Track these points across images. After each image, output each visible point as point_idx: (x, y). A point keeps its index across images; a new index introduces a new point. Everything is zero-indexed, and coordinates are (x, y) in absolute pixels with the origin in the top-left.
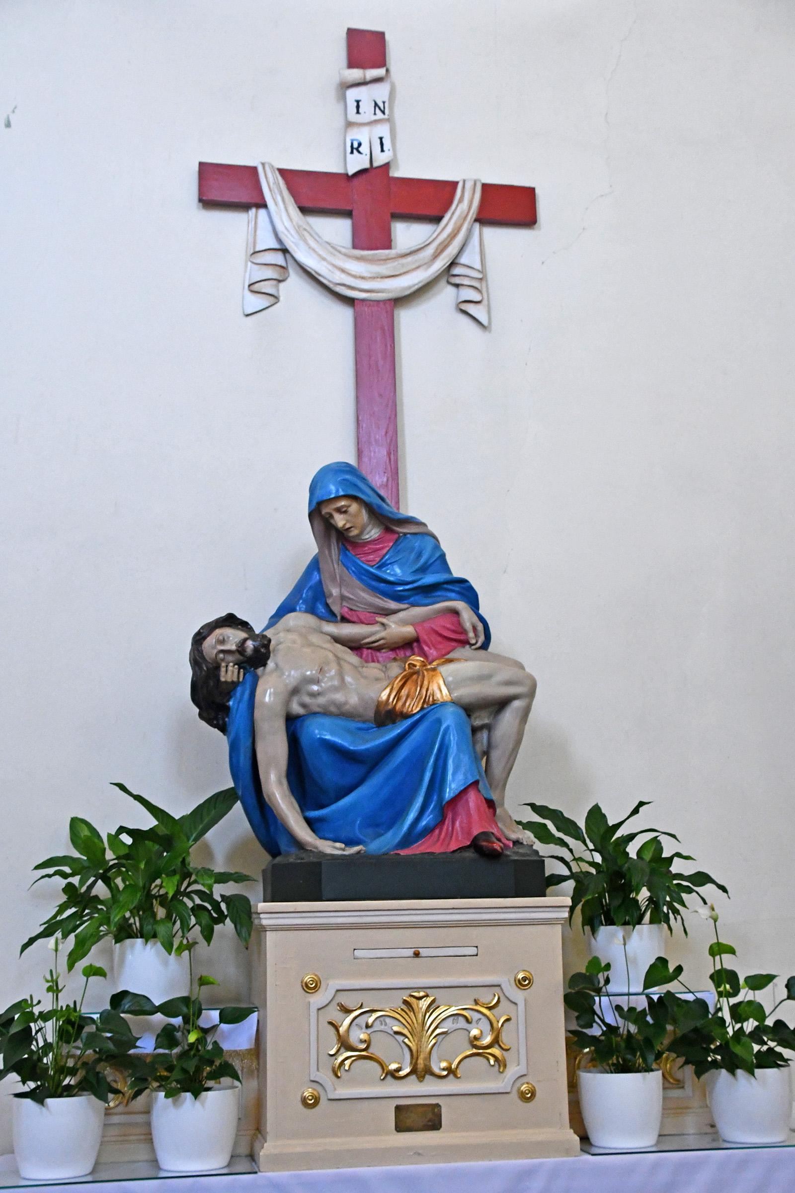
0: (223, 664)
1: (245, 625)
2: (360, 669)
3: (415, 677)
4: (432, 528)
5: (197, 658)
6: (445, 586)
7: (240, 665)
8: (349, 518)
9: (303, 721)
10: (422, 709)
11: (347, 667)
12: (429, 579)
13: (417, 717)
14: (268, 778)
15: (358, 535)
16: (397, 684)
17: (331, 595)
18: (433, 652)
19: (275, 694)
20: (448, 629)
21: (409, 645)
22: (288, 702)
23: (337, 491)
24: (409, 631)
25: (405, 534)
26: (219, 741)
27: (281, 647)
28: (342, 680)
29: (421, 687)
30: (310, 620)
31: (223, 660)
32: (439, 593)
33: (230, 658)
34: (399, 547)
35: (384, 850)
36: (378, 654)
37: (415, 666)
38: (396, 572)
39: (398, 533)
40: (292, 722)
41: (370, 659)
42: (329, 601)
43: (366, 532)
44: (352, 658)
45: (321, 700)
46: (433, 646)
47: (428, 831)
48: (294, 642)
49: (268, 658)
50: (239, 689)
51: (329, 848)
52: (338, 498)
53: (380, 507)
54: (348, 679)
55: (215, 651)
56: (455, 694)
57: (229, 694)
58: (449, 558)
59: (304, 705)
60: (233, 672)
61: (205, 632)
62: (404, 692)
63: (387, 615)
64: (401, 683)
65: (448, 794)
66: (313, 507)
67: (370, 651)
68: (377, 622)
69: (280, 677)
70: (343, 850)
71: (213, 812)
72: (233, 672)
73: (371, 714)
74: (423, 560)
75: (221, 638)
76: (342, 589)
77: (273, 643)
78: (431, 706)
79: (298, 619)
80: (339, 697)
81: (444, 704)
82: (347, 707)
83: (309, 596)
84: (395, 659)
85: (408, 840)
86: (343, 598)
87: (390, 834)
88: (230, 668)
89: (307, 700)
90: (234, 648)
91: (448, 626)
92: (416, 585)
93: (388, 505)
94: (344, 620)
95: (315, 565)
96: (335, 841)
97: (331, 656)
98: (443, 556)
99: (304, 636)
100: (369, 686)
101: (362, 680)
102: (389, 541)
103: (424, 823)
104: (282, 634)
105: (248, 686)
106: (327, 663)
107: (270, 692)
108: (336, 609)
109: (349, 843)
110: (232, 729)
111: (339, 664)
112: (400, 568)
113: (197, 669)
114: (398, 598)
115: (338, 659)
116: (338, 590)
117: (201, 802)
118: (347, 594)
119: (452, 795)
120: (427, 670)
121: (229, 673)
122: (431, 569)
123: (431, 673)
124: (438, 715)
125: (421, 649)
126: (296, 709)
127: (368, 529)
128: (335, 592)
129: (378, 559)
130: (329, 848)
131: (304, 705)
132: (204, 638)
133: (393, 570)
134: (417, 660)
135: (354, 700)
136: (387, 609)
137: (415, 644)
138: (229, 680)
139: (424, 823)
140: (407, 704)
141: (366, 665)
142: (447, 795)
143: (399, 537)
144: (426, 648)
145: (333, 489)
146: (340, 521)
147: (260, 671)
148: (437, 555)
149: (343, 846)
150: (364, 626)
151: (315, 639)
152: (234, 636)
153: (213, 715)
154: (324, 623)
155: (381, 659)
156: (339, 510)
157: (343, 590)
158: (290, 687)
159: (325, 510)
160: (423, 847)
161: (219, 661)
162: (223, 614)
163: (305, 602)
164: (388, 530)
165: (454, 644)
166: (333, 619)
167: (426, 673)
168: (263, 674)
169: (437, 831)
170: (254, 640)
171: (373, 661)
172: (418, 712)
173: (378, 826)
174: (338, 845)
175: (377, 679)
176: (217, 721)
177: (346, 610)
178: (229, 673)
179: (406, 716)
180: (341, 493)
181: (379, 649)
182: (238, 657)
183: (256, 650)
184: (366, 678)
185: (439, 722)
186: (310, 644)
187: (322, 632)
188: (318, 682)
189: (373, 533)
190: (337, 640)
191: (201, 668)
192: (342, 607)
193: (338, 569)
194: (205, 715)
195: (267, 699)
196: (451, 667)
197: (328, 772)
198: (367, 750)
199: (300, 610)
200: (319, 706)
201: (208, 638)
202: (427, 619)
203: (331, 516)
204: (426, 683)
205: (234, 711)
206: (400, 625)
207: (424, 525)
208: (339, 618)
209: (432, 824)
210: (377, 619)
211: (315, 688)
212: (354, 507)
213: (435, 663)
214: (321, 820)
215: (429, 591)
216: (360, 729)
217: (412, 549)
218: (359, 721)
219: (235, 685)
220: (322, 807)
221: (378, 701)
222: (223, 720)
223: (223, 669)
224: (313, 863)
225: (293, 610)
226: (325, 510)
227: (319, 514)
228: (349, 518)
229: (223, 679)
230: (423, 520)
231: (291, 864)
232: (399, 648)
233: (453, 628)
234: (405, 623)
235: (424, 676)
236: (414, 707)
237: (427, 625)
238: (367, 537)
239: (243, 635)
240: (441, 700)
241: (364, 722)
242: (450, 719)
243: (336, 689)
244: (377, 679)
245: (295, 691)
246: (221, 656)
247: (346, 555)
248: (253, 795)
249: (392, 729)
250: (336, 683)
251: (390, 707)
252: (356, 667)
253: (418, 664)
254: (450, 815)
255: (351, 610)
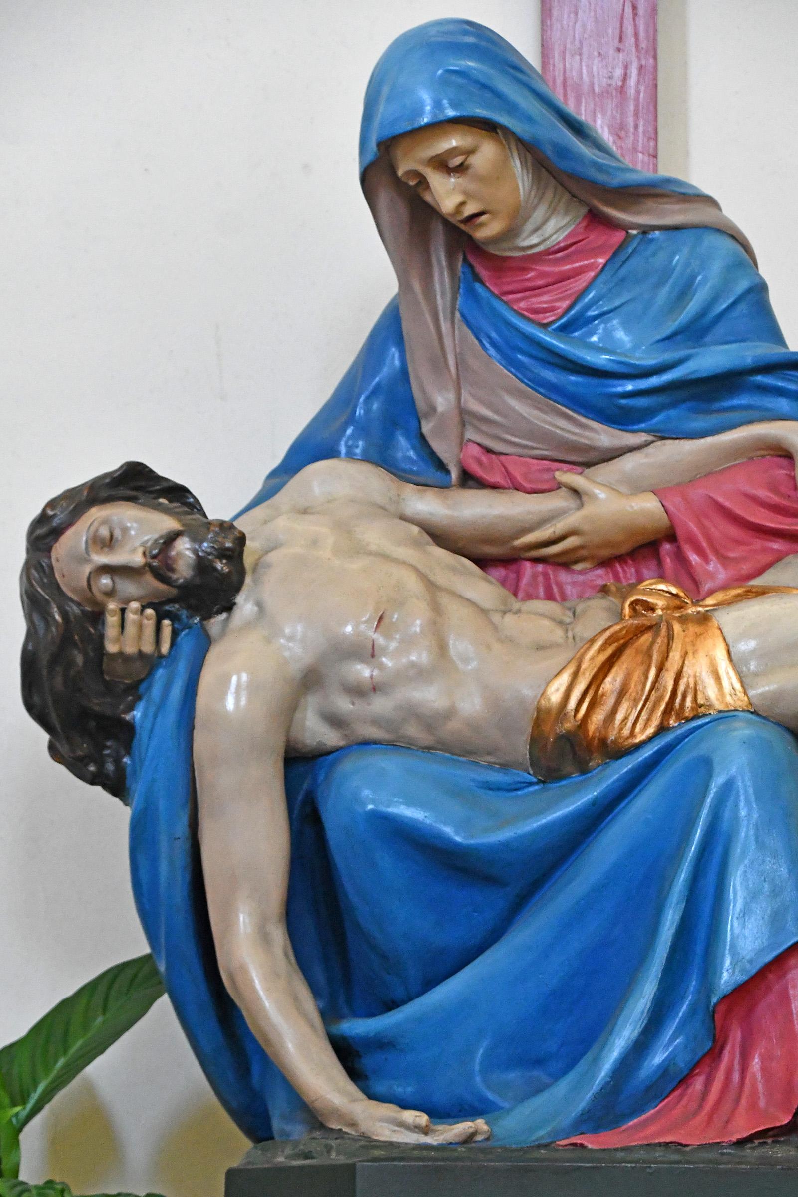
0: (112, 606)
1: (178, 495)
2: (496, 618)
3: (646, 639)
4: (735, 211)
5: (40, 589)
6: (759, 378)
7: (160, 608)
8: (472, 186)
9: (333, 764)
10: (662, 729)
11: (456, 612)
12: (710, 359)
13: (647, 753)
14: (229, 924)
15: (496, 240)
16: (593, 659)
17: (433, 409)
18: (715, 570)
19: (253, 688)
20: (754, 499)
21: (647, 549)
22: (290, 709)
23: (438, 105)
24: (646, 508)
25: (645, 230)
26: (113, 816)
27: (272, 557)
28: (442, 648)
29: (660, 669)
30: (370, 481)
31: (111, 593)
32: (742, 400)
33: (128, 587)
34: (623, 272)
35: (542, 1133)
36: (564, 576)
37: (651, 608)
38: (617, 341)
39: (624, 227)
40: (303, 770)
41: (541, 591)
42: (427, 428)
43: (529, 226)
44: (482, 588)
45: (380, 705)
46: (717, 552)
47: (673, 1081)
48: (314, 543)
49: (238, 588)
50: (160, 673)
51: (389, 1125)
52: (440, 126)
53: (563, 152)
54: (458, 646)
55: (87, 569)
56: (762, 688)
57: (134, 691)
58: (776, 301)
59: (335, 721)
60: (140, 627)
61: (60, 517)
62: (611, 684)
63: (588, 465)
64: (603, 657)
65: (728, 976)
66: (370, 157)
67: (540, 567)
68: (559, 486)
69: (268, 640)
70: (426, 1131)
71: (100, 1020)
72: (140, 627)
73: (520, 747)
74: (692, 307)
75: (104, 532)
76: (470, 392)
77: (252, 545)
78: (684, 720)
79: (339, 480)
80: (430, 696)
81: (726, 715)
82: (453, 725)
83: (377, 417)
84: (604, 590)
85: (608, 1110)
86: (465, 417)
87: (562, 1087)
88: (131, 617)
89: (344, 705)
90: (138, 559)
91: (762, 493)
92: (667, 377)
93: (598, 145)
94: (468, 479)
95: (390, 329)
96: (405, 1105)
97: (413, 583)
98: (758, 292)
99: (343, 527)
100: (518, 662)
101: (497, 647)
102: (596, 252)
103: (658, 1058)
104: (282, 523)
105: (182, 667)
106: (399, 603)
107: (238, 681)
108: (444, 449)
109: (440, 1113)
110: (138, 788)
111: (437, 609)
112: (627, 329)
113: (36, 618)
114: (620, 417)
115: (432, 586)
116: (452, 396)
117: (69, 992)
118: (474, 406)
119: (741, 978)
120: (683, 620)
121: (130, 632)
122: (720, 330)
123: (693, 629)
124: (703, 749)
125: (681, 558)
126: (315, 731)
127: (539, 214)
128: (443, 401)
129: (565, 304)
130: (389, 1125)
131: (335, 721)
132: (57, 532)
133: (608, 334)
134: (658, 591)
135: (471, 704)
136: (589, 449)
137: (667, 547)
138: (130, 649)
139: (658, 1058)
140: (620, 716)
141: (516, 605)
142: (725, 976)
143: (629, 238)
144: (694, 558)
145: (428, 105)
146: (447, 193)
147: (216, 623)
148: (742, 285)
149: (423, 1119)
150: (520, 495)
151: (375, 534)
152: (139, 528)
153: (84, 748)
154: (409, 489)
155: (568, 589)
156: (442, 163)
157: (465, 395)
158: (295, 669)
159: (406, 164)
160: (653, 1129)
161: (99, 597)
162: (112, 464)
163: (363, 430)
164: (596, 219)
165: (776, 545)
166: (434, 475)
167: (677, 627)
168: (223, 633)
169: (698, 1084)
170: (196, 539)
171: (550, 597)
172: (650, 739)
173: (538, 1063)
174: (410, 1116)
175: (540, 648)
176: (101, 764)
177: (475, 450)
178: (131, 630)
179: (618, 752)
180: (451, 113)
181: (564, 562)
182: (150, 581)
183: (202, 565)
184: (509, 641)
185: (706, 765)
186: (359, 550)
187: (403, 518)
188: (371, 654)
189: (551, 228)
190: (440, 536)
191: (46, 617)
192: (463, 443)
193: (455, 337)
194: (64, 749)
195: (230, 703)
196: (754, 611)
197: (392, 906)
198: (505, 846)
199: (350, 455)
200: (376, 722)
201: (70, 532)
202: (707, 473)
203: (423, 182)
204: (675, 656)
205: (145, 740)
206: (620, 494)
207: (710, 201)
208: (454, 475)
209: (683, 1063)
210: (558, 475)
211: (364, 672)
212: (487, 154)
213: (710, 601)
214: (381, 1043)
215: (712, 393)
216: (490, 787)
217: (666, 272)
218: (490, 766)
219: (150, 663)
220: (391, 1005)
221: (539, 710)
222: (117, 761)
223: (112, 620)
224: (333, 1169)
225: (330, 453)
226: (406, 164)
227: (386, 171)
228: (472, 186)
229: (112, 648)
230: (707, 190)
231: (280, 1170)
232: (620, 558)
233: (775, 499)
234: (637, 487)
235: (670, 637)
236: (634, 723)
237: (698, 493)
238: (534, 240)
239: (169, 523)
240: (719, 706)
241: (505, 767)
242: (735, 760)
243: (421, 674)
244: (540, 648)
245: (310, 680)
246: (105, 581)
247: (471, 294)
248: (198, 971)
249: (578, 789)
250: (420, 656)
251: (568, 725)
252: (484, 612)
253: (660, 603)
254: (736, 1036)
255: (489, 451)
